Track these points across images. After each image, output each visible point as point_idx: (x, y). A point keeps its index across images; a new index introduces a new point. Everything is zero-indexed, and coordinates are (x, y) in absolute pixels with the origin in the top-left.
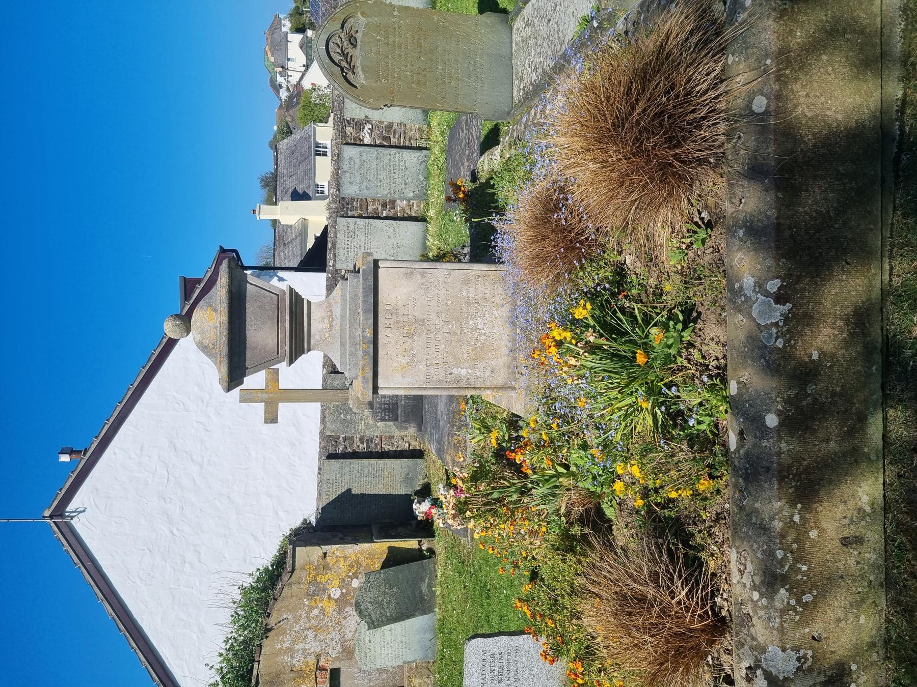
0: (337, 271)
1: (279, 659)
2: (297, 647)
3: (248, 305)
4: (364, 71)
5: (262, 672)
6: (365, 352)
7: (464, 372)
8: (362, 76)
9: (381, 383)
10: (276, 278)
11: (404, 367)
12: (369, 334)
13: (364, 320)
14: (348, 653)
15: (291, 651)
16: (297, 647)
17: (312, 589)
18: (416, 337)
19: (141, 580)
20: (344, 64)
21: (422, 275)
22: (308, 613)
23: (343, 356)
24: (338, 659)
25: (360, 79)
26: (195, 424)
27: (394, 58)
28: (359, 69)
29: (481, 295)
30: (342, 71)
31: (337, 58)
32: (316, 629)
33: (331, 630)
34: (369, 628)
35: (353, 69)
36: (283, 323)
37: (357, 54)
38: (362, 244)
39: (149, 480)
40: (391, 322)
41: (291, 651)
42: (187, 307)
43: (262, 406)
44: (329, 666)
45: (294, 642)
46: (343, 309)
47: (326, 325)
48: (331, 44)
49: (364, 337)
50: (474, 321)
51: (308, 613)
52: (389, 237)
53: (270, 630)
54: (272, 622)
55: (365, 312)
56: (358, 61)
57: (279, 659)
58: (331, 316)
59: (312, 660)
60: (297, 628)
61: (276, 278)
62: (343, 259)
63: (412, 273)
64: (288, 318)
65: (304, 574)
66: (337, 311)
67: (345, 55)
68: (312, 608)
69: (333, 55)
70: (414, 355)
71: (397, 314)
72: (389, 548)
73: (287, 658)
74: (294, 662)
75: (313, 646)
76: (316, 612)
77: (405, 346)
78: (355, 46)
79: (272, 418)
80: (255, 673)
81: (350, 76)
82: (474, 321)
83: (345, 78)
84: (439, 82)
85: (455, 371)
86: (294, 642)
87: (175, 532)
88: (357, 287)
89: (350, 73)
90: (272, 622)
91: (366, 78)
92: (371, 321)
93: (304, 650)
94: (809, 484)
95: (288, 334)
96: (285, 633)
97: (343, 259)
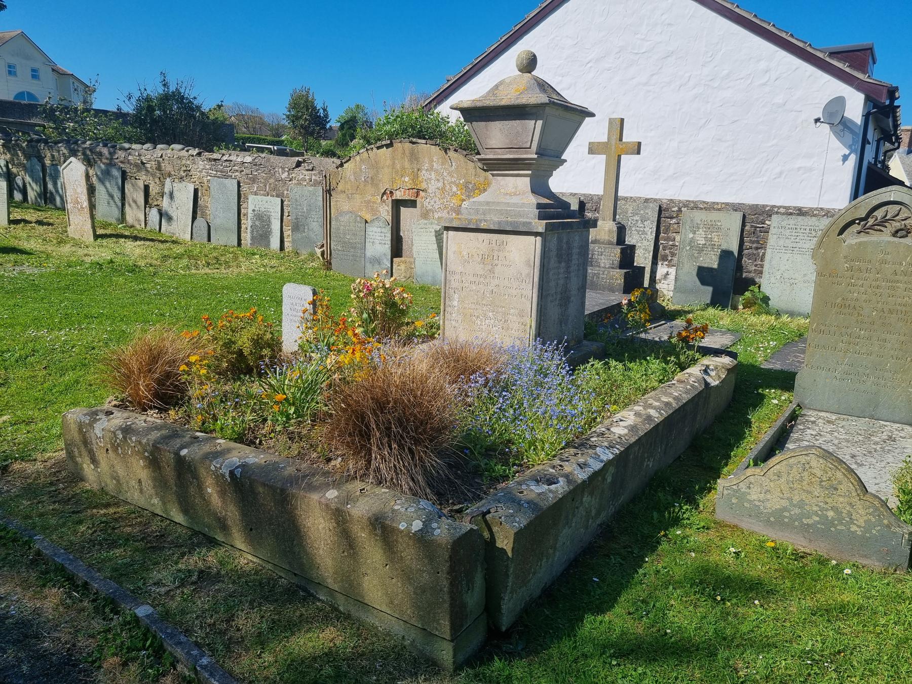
0: (770, 216)
1: (426, 160)
2: (433, 173)
3: (518, 121)
4: (860, 244)
5: (420, 146)
6: (470, 221)
7: (455, 303)
8: (854, 242)
9: (451, 233)
10: (847, 152)
11: (461, 253)
12: (483, 225)
13: (492, 220)
14: (425, 215)
15: (431, 168)
16: (433, 173)
17: (470, 186)
18: (482, 266)
19: (553, 39)
20: (871, 221)
21: (528, 275)
22: (454, 183)
23: (480, 203)
24: (423, 206)
25: (852, 238)
26: (687, 75)
27: (877, 280)
28: (863, 238)
29: (511, 326)
30: (861, 220)
31: (879, 214)
32: (443, 189)
33: (442, 201)
34: (436, 232)
35: (864, 231)
36: (510, 153)
37: (885, 237)
38: (799, 245)
39: (639, 36)
40: (494, 244)
41: (431, 168)
42: (820, 55)
43: (604, 139)
44: (418, 200)
45: (436, 171)
46: (515, 205)
47: (511, 189)
48: (898, 207)
49: (481, 221)
50: (492, 317)
51: (454, 183)
52: (805, 275)
53: (446, 152)
54: (451, 153)
55: (499, 223)
56: (874, 237)
57: (426, 160)
58: (515, 194)
59: (423, 186)
60: (445, 174)
61: (847, 152)
62: (784, 224)
63: (530, 266)
64: (511, 156)
65: (482, 179)
66: (514, 200)
67: (884, 222)
68: (457, 186)
69: (884, 209)
70: (469, 262)
71: (499, 251)
72: (643, 269)
73: (426, 166)
74: (424, 172)
75: (433, 187)
76: (454, 189)
77: (476, 255)
78: (895, 234)
79: (637, 149)
80: (419, 141)
81: (855, 228)
82: (492, 317)
83: (852, 223)
84: (844, 330)
85: (456, 296)
86: (436, 171)
87: (589, 65)
88: (527, 217)
89: (859, 228)
90: (451, 153)
91: (851, 246)
92: (492, 227)
93: (430, 179)
94: (154, 462)
95: (499, 157)
96: (443, 164)
97: (784, 224)
